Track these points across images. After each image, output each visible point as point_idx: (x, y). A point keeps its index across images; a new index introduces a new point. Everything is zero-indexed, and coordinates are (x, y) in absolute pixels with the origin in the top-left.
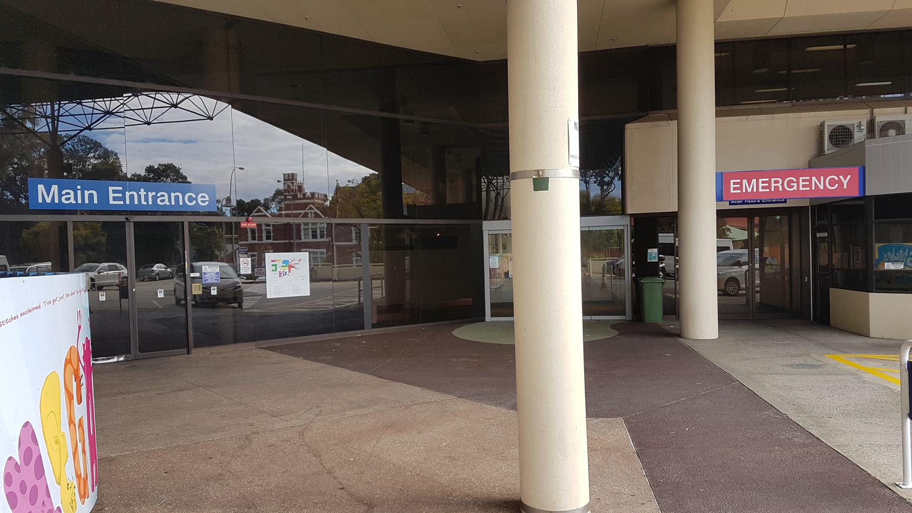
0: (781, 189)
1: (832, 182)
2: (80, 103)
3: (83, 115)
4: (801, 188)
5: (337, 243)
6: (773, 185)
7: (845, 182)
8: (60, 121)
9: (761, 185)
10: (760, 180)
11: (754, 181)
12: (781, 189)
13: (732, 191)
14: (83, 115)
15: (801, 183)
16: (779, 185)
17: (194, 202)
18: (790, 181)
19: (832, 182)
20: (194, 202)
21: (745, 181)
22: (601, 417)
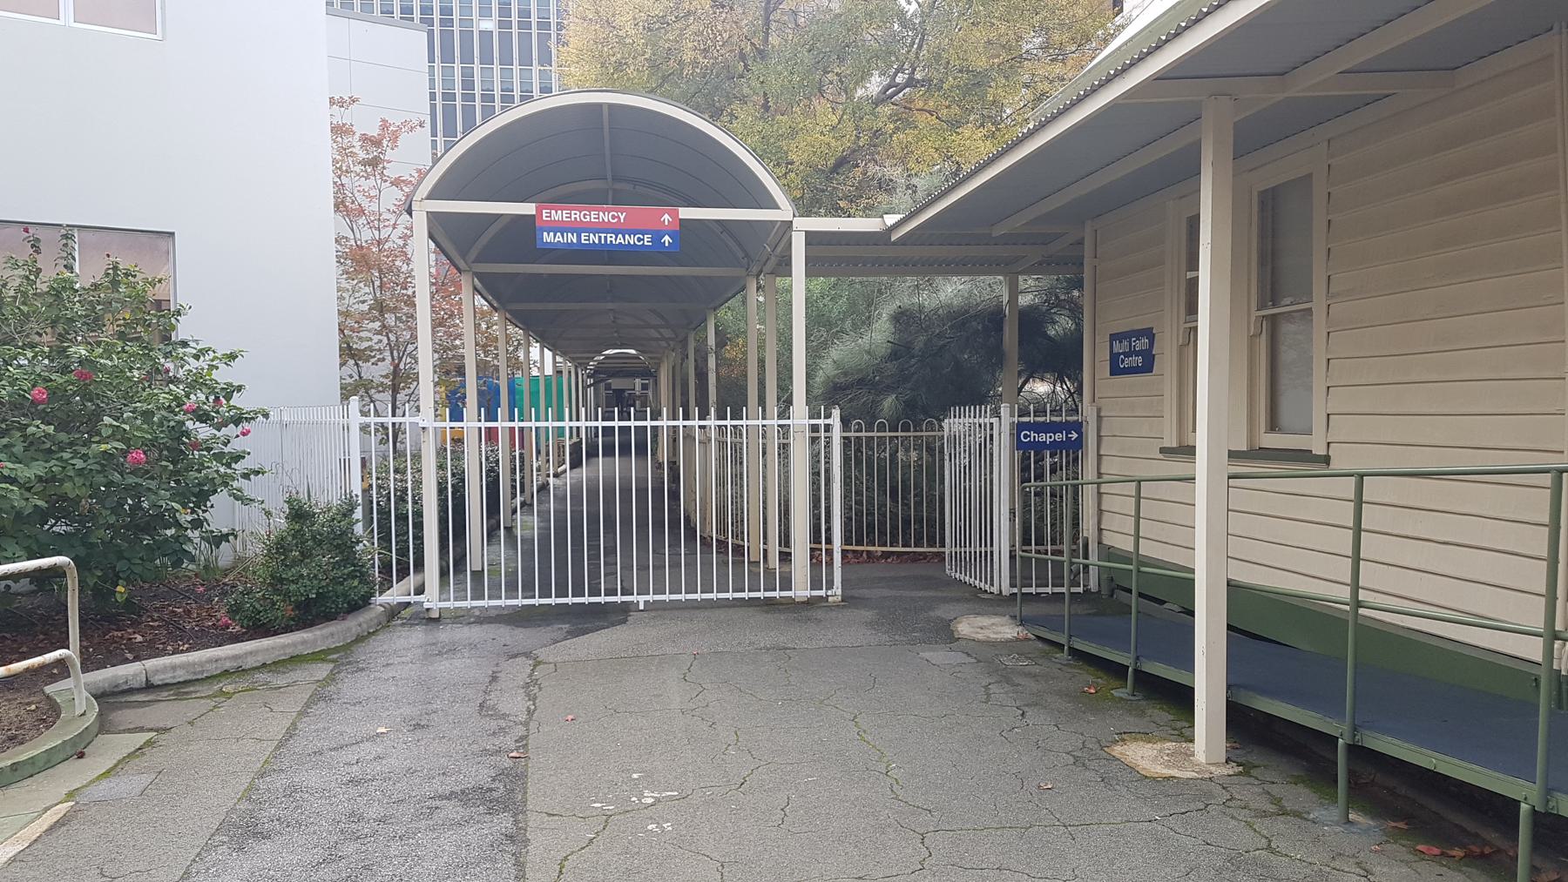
0: (578, 219)
1: (613, 217)
2: (370, 604)
3: (1232, 558)
4: (593, 220)
5: (1131, 567)
6: (573, 216)
7: (622, 218)
8: (1365, 502)
9: (564, 215)
10: (564, 212)
11: (559, 212)
12: (578, 219)
13: (544, 218)
14: (1232, 558)
15: (593, 216)
16: (577, 216)
17: (616, 220)
18: (585, 215)
19: (613, 217)
20: (616, 220)
21: (553, 212)
22: (979, 641)
